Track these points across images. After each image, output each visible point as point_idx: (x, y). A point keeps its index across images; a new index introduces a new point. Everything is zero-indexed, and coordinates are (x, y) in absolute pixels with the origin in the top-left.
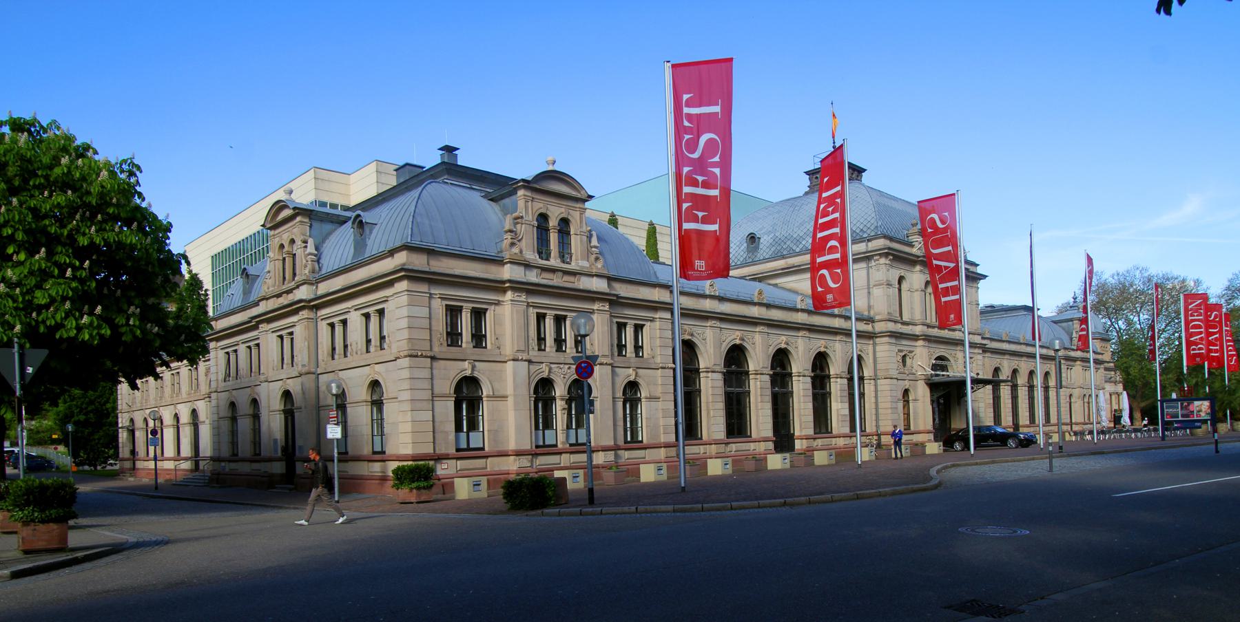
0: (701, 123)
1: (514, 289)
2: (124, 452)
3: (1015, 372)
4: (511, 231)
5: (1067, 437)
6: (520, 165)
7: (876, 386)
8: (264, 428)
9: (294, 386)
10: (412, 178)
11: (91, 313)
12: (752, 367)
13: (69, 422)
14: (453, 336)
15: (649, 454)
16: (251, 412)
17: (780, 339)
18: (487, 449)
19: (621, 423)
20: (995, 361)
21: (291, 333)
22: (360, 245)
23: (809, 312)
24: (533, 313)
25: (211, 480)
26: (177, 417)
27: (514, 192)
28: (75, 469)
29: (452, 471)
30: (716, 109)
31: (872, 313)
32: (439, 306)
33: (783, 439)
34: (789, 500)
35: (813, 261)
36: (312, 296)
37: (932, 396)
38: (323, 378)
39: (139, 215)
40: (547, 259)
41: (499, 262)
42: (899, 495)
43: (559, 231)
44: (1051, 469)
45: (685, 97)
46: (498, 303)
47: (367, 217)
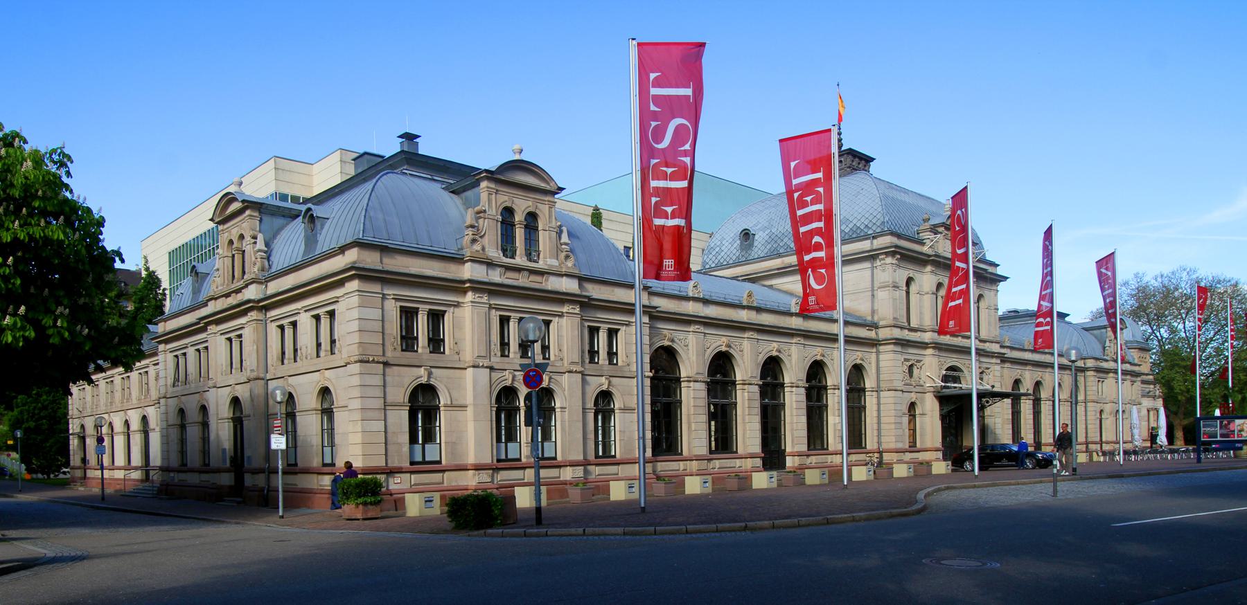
0: (671, 107)
1: (474, 290)
2: (75, 460)
3: (1038, 384)
4: (472, 226)
5: (1095, 458)
6: (485, 156)
7: (878, 398)
8: (212, 436)
9: (243, 392)
10: (370, 167)
11: (15, 314)
12: (787, 380)
13: (286, 452)
14: (408, 341)
15: (623, 470)
16: (200, 419)
17: (771, 346)
18: (444, 462)
19: (592, 436)
20: (1016, 372)
21: (240, 336)
22: (311, 241)
23: (1032, 351)
24: (495, 315)
25: (160, 491)
26: (127, 423)
27: (476, 184)
28: (27, 477)
29: (406, 486)
30: (688, 92)
31: (876, 319)
32: (392, 308)
33: (772, 456)
34: (751, 524)
35: (800, 260)
36: (262, 296)
37: (941, 410)
38: (272, 384)
39: (67, 209)
40: (513, 257)
41: (459, 260)
42: (896, 520)
43: (526, 227)
44: (1055, 492)
45: (652, 76)
46: (457, 305)
47: (318, 211)
